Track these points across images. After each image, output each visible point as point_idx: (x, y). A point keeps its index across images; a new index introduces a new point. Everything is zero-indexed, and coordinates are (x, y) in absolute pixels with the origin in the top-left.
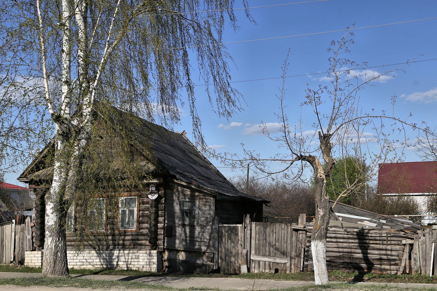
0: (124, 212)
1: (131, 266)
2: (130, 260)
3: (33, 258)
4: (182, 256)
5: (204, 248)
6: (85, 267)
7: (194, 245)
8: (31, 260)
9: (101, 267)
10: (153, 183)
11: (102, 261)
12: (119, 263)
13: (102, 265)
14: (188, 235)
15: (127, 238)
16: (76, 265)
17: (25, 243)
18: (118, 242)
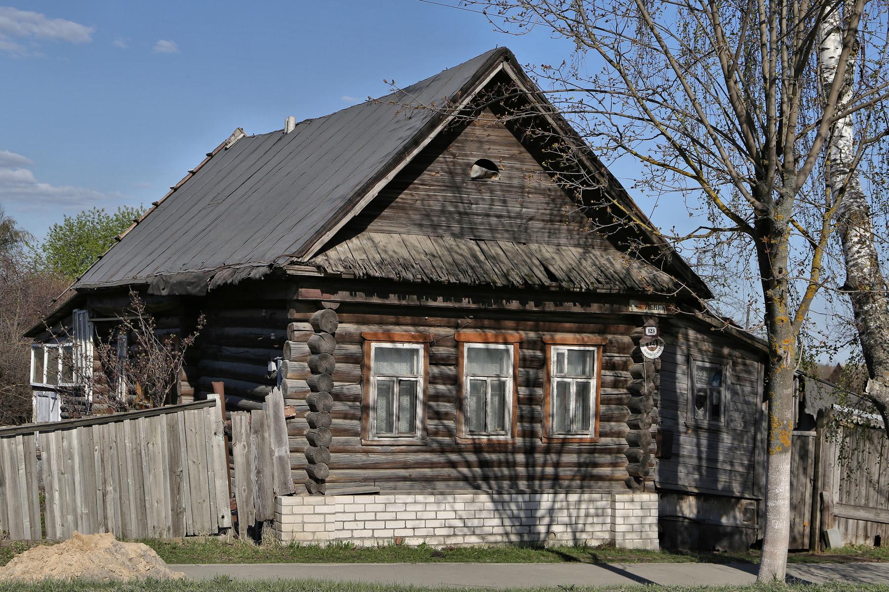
0: (563, 387)
1: (584, 536)
2: (581, 521)
3: (307, 519)
4: (689, 508)
5: (737, 489)
6: (459, 540)
7: (716, 481)
8: (303, 523)
9: (505, 539)
10: (652, 316)
11: (507, 522)
12: (555, 528)
13: (507, 534)
14: (704, 455)
15: (566, 458)
16: (435, 536)
17: (267, 471)
18: (543, 471)
